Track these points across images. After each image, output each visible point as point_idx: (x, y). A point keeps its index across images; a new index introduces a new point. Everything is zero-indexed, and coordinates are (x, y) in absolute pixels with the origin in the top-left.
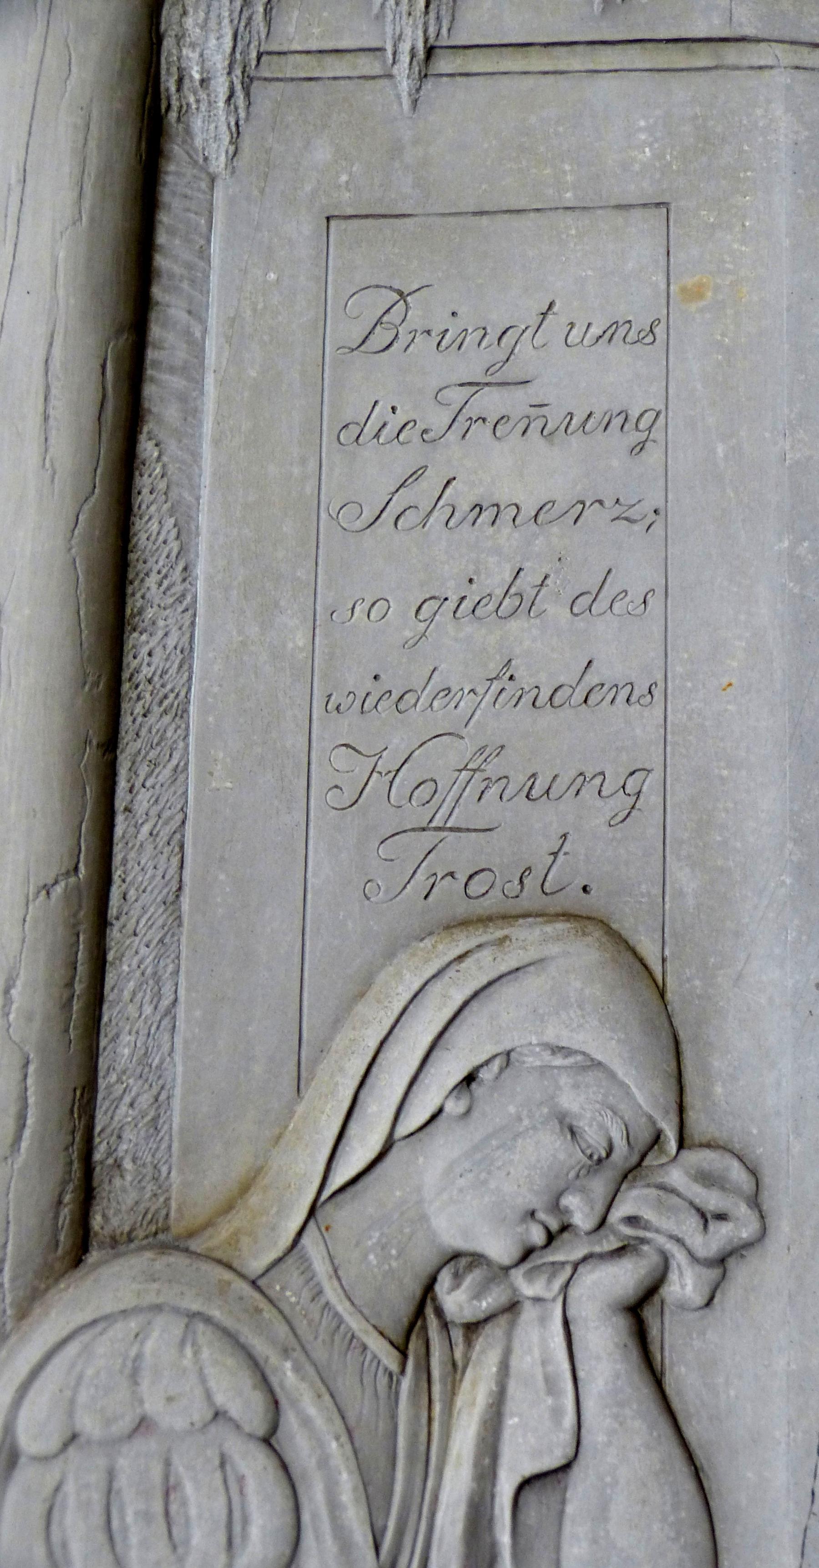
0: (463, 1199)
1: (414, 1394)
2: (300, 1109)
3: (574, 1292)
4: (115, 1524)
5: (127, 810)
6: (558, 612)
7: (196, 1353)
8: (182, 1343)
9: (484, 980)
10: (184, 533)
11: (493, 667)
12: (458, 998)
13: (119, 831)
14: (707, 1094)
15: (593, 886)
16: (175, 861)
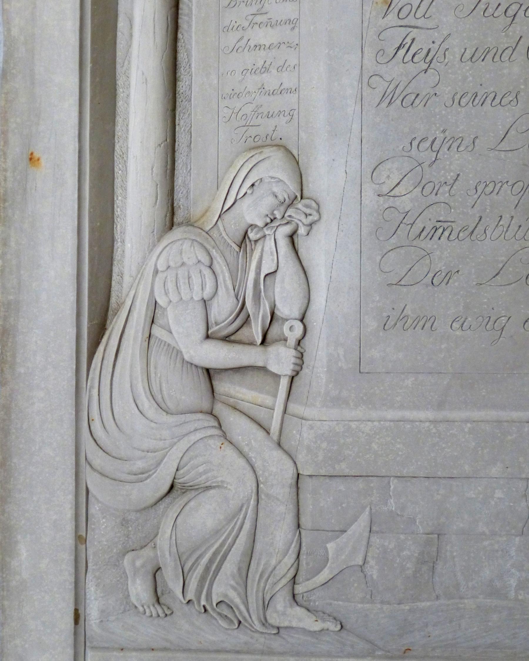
0: (251, 212)
1: (243, 256)
2: (218, 193)
3: (277, 233)
4: (178, 284)
5: (179, 125)
6: (274, 71)
7: (194, 248)
8: (191, 246)
9: (256, 162)
10: (189, 56)
11: (260, 86)
12: (250, 166)
13: (177, 130)
14: (308, 187)
15: (282, 138)
16: (190, 136)
